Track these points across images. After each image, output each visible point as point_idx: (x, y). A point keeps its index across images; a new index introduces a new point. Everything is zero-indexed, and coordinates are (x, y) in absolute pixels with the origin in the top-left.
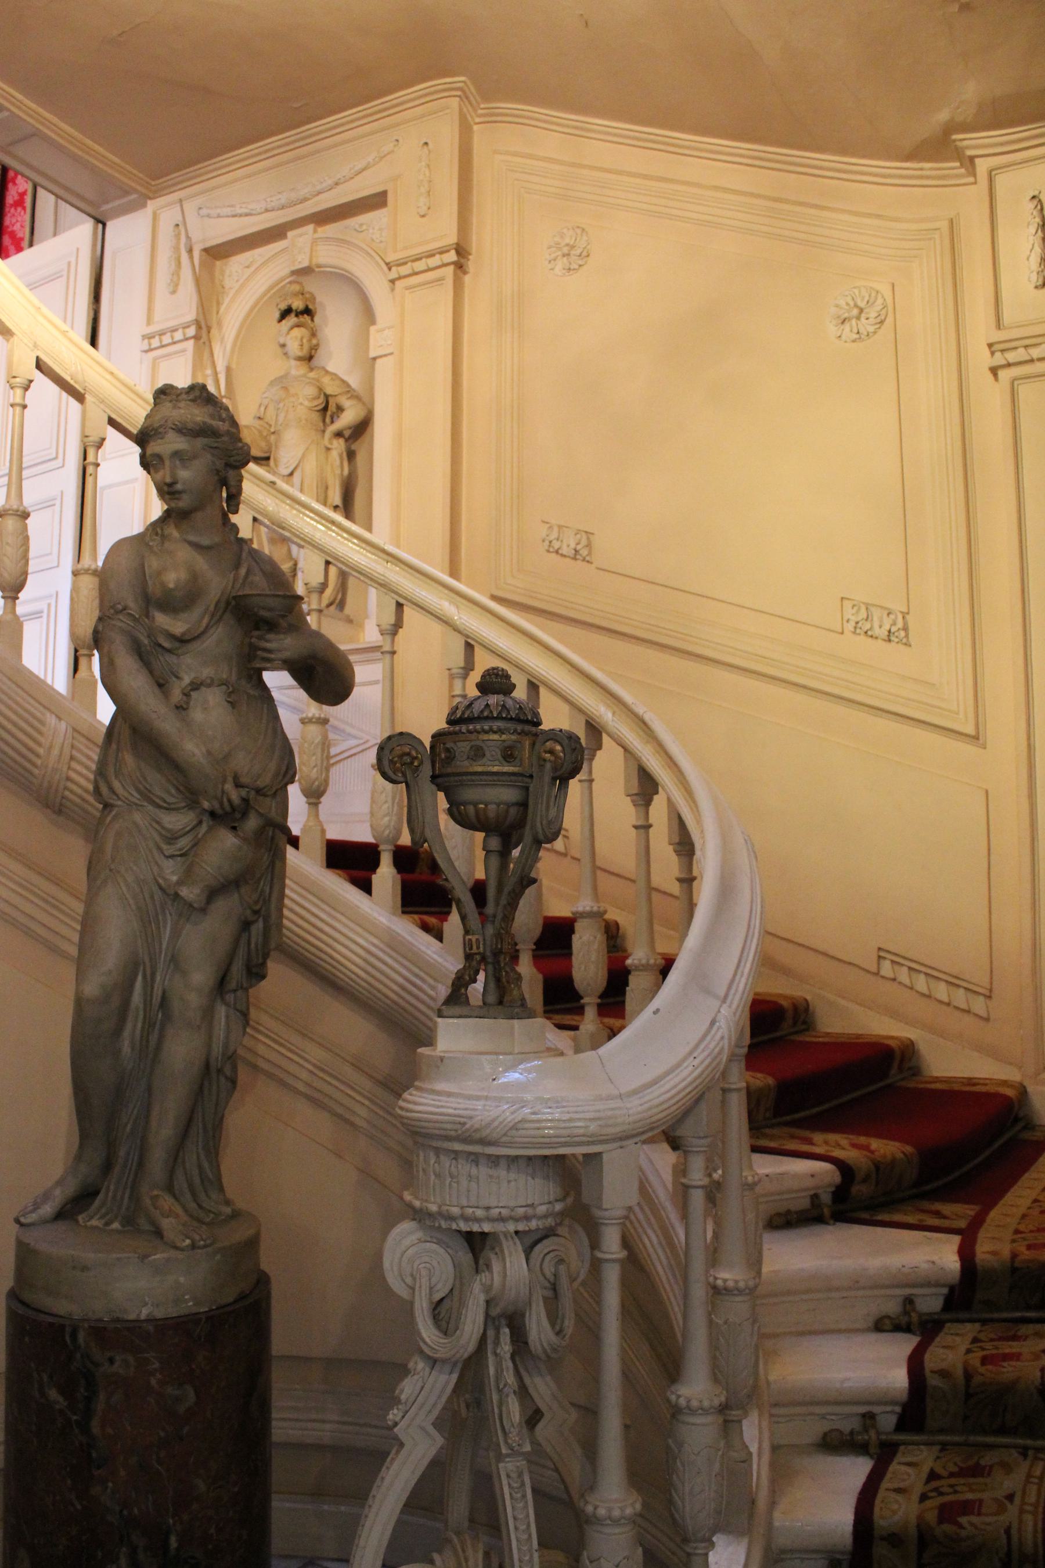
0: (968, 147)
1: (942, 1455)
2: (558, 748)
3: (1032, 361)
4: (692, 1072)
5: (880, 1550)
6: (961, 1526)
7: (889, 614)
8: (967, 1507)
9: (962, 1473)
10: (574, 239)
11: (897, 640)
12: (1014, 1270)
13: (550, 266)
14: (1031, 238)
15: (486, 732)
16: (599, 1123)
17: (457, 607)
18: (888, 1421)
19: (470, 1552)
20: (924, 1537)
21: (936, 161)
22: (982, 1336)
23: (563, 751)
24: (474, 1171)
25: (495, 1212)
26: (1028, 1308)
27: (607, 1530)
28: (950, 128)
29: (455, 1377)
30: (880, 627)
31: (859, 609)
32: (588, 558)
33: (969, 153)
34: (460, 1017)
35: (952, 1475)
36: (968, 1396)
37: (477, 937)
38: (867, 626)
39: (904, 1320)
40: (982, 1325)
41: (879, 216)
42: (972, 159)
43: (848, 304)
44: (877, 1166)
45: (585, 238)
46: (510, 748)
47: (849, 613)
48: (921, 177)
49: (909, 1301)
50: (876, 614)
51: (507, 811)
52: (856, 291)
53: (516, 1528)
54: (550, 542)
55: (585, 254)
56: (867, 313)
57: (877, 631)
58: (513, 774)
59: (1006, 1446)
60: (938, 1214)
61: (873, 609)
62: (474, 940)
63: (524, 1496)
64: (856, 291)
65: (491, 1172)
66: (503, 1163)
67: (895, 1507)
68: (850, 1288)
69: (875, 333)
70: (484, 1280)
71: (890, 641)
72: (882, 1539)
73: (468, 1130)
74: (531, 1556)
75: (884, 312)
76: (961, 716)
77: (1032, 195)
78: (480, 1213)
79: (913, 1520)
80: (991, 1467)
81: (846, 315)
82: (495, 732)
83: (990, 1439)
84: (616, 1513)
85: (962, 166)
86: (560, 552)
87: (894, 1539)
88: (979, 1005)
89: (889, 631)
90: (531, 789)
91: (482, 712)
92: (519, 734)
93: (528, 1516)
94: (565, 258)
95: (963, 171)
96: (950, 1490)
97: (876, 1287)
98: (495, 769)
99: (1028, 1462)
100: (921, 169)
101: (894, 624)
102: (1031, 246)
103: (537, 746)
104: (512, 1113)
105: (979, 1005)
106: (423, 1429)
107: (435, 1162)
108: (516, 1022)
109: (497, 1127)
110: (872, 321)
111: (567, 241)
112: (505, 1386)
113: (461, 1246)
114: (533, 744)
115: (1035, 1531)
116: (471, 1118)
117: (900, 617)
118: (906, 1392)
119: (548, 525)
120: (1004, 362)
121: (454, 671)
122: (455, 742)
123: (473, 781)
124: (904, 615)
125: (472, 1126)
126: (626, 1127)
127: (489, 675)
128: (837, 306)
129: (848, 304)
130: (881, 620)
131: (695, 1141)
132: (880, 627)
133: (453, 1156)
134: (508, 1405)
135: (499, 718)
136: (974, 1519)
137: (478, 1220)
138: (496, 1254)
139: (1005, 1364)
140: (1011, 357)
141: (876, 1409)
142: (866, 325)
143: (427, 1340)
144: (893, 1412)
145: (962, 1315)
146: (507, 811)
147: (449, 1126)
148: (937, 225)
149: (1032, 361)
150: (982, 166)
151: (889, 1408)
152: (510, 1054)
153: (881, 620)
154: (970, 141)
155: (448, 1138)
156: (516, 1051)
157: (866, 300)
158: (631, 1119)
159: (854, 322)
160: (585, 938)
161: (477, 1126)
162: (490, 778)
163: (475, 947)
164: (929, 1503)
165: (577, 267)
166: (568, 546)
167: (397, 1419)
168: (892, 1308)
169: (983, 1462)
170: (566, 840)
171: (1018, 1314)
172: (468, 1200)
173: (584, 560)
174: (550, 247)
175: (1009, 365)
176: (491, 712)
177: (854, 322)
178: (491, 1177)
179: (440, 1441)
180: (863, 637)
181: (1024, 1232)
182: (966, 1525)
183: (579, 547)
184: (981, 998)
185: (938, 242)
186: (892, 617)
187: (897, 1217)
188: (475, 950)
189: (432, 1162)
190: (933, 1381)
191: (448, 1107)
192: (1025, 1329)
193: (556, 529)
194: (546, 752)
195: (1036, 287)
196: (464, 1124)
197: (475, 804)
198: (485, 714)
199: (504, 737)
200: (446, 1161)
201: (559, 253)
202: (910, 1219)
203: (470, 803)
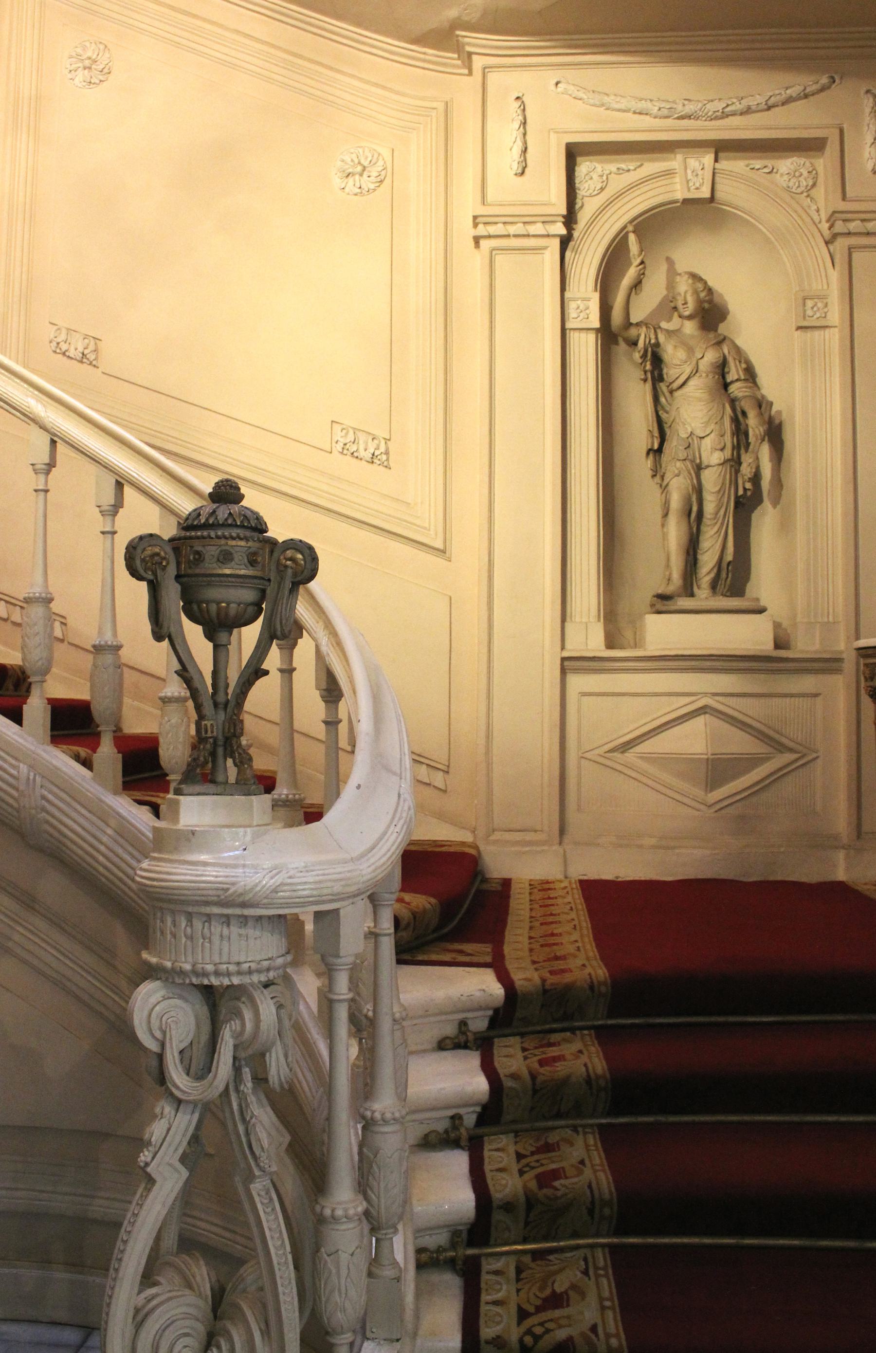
0: (469, 44)
1: (518, 1139)
2: (300, 556)
3: (508, 236)
4: (397, 838)
5: (498, 1216)
6: (557, 1189)
7: (373, 439)
8: (556, 1174)
9: (538, 1151)
10: (96, 53)
11: (379, 462)
12: (545, 991)
13: (70, 76)
14: (515, 132)
15: (233, 538)
16: (342, 883)
17: (44, 406)
18: (470, 1120)
19: (195, 1269)
20: (530, 1202)
21: (438, 50)
22: (526, 1045)
23: (304, 560)
24: (226, 931)
25: (245, 966)
26: (555, 1020)
27: (344, 1227)
28: (457, 24)
29: (196, 1116)
30: (366, 450)
31: (347, 434)
32: (94, 363)
33: (469, 49)
34: (198, 794)
35: (533, 1153)
36: (535, 1091)
37: (212, 722)
38: (354, 448)
39: (462, 1039)
40: (522, 1038)
41: (384, 88)
42: (470, 54)
43: (352, 161)
44: (414, 914)
45: (107, 55)
46: (255, 554)
47: (338, 435)
48: (424, 61)
49: (463, 1023)
50: (362, 437)
51: (245, 611)
52: (361, 150)
53: (272, 1238)
54: (58, 343)
55: (106, 70)
56: (370, 172)
57: (362, 453)
58: (255, 577)
59: (562, 1127)
60: (461, 952)
61: (359, 434)
62: (209, 725)
63: (274, 1209)
64: (361, 150)
65: (243, 931)
66: (251, 923)
67: (504, 1182)
68: (421, 1017)
69: (374, 190)
70: (234, 1028)
71: (373, 462)
72: (500, 1207)
73: (231, 895)
74: (286, 1259)
75: (383, 173)
76: (432, 532)
77: (517, 95)
78: (232, 968)
79: (521, 1191)
80: (558, 1143)
81: (351, 170)
82: (241, 539)
83: (550, 1123)
84: (351, 1212)
85: (459, 58)
86: (67, 354)
87: (508, 1207)
88: (438, 779)
89: (373, 455)
90: (268, 592)
91: (226, 520)
92: (261, 542)
93: (279, 1225)
94: (86, 71)
95: (459, 62)
96: (537, 1164)
97: (441, 1013)
98: (242, 572)
99: (581, 1136)
100: (424, 53)
101: (377, 448)
102: (514, 139)
103: (276, 554)
104: (272, 878)
105: (438, 779)
106: (170, 1165)
107: (187, 926)
108: (253, 797)
109: (260, 891)
110: (372, 179)
111: (89, 54)
112: (251, 1118)
113: (197, 998)
114: (272, 552)
115: (609, 1183)
116: (233, 884)
117: (383, 442)
118: (488, 1093)
119: (56, 327)
120: (486, 234)
121: (38, 467)
122: (204, 546)
123: (221, 582)
124: (387, 440)
125: (235, 892)
126: (360, 886)
127: (220, 487)
128: (343, 161)
129: (352, 161)
130: (366, 443)
131: (387, 896)
132: (366, 450)
133: (205, 919)
134: (256, 1134)
135: (242, 526)
136: (562, 1181)
137: (229, 974)
138: (244, 1003)
139: (556, 1064)
140: (492, 230)
141: (462, 1111)
142: (367, 183)
143: (181, 1086)
144: (473, 1112)
145: (507, 1031)
146: (245, 611)
147: (210, 892)
148: (434, 105)
149: (508, 236)
150: (478, 62)
151: (472, 1109)
152: (249, 826)
153: (366, 443)
154: (472, 40)
155: (207, 903)
156: (255, 823)
157: (369, 159)
158: (365, 879)
159: (357, 177)
160: (173, 721)
161: (240, 891)
162: (238, 580)
163: (209, 732)
164: (526, 1176)
165: (98, 82)
166: (76, 349)
167: (149, 1159)
168: (450, 1030)
169: (550, 1141)
170: (64, 627)
171: (547, 1026)
172: (220, 958)
173: (91, 364)
174: (71, 57)
175: (489, 237)
176: (235, 520)
177: (357, 177)
178: (240, 935)
179: (185, 1173)
180: (349, 458)
181: (539, 962)
182: (559, 1187)
183: (86, 352)
184: (441, 773)
185: (434, 120)
186: (376, 441)
187: (434, 957)
188: (209, 734)
189: (183, 925)
190: (508, 1083)
191: (209, 876)
192: (555, 1037)
193: (64, 332)
194: (287, 559)
195: (516, 174)
196: (228, 889)
197: (218, 603)
198: (230, 521)
199: (250, 544)
200: (198, 924)
201: (80, 65)
202: (447, 957)
203: (214, 601)
